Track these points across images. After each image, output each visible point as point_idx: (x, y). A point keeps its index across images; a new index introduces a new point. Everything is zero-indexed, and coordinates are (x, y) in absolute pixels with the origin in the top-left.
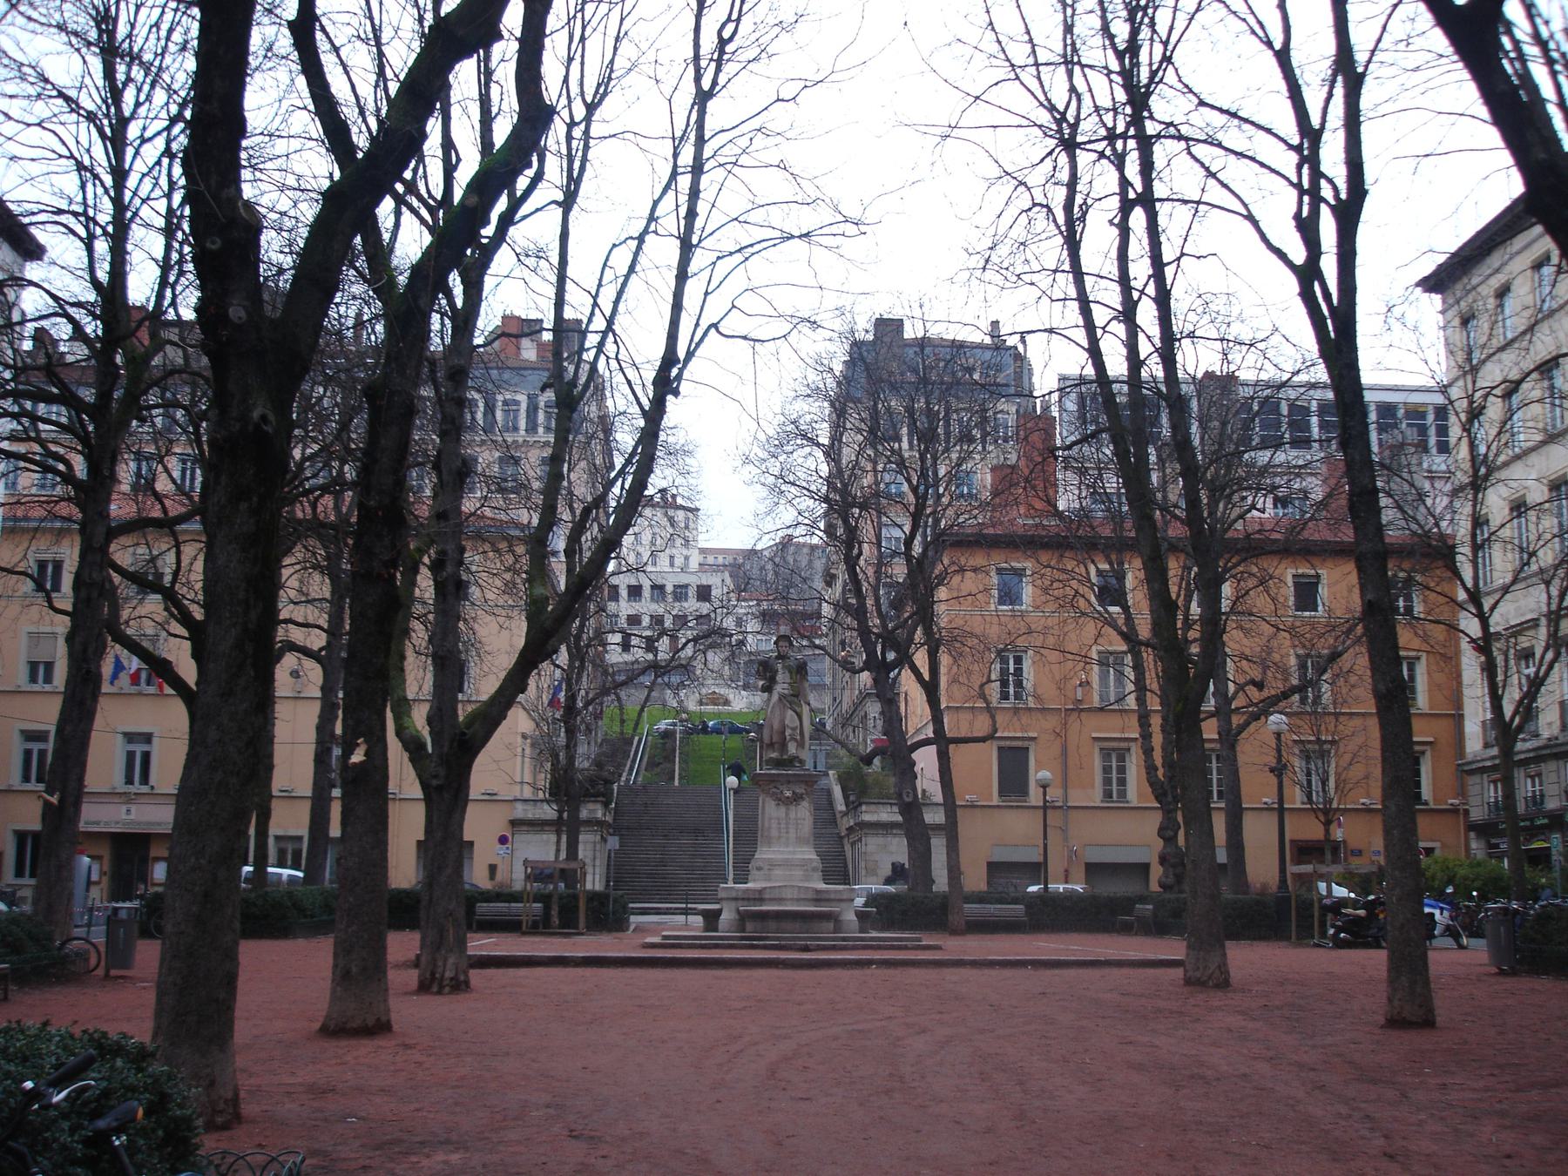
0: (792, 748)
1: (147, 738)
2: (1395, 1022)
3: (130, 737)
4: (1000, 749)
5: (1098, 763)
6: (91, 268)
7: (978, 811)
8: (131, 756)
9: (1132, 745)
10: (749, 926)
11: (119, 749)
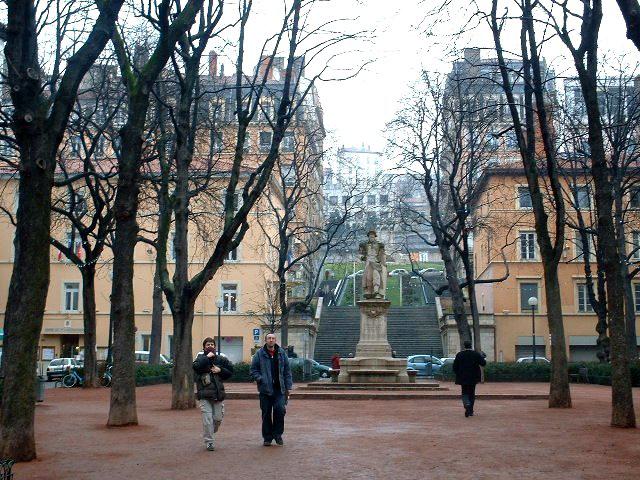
0: (376, 289)
1: (234, 287)
2: (615, 425)
3: (227, 287)
4: (522, 284)
5: (576, 292)
6: (12, 220)
7: (510, 318)
8: (69, 294)
9: (539, 282)
10: (353, 379)
11: (64, 291)
